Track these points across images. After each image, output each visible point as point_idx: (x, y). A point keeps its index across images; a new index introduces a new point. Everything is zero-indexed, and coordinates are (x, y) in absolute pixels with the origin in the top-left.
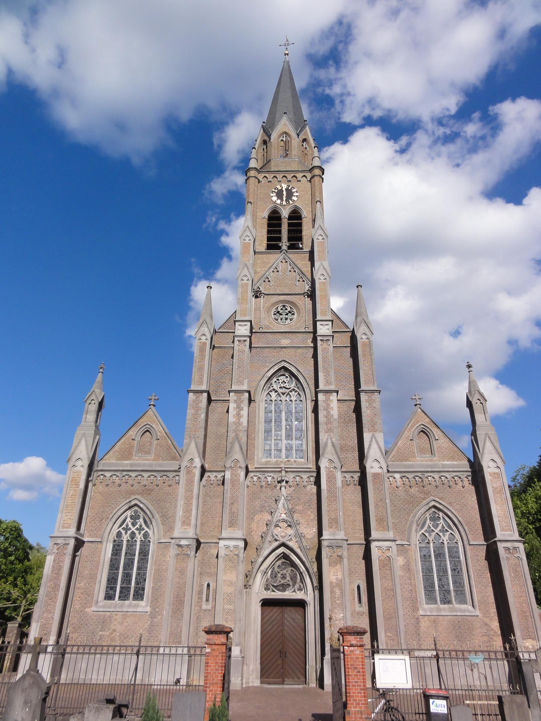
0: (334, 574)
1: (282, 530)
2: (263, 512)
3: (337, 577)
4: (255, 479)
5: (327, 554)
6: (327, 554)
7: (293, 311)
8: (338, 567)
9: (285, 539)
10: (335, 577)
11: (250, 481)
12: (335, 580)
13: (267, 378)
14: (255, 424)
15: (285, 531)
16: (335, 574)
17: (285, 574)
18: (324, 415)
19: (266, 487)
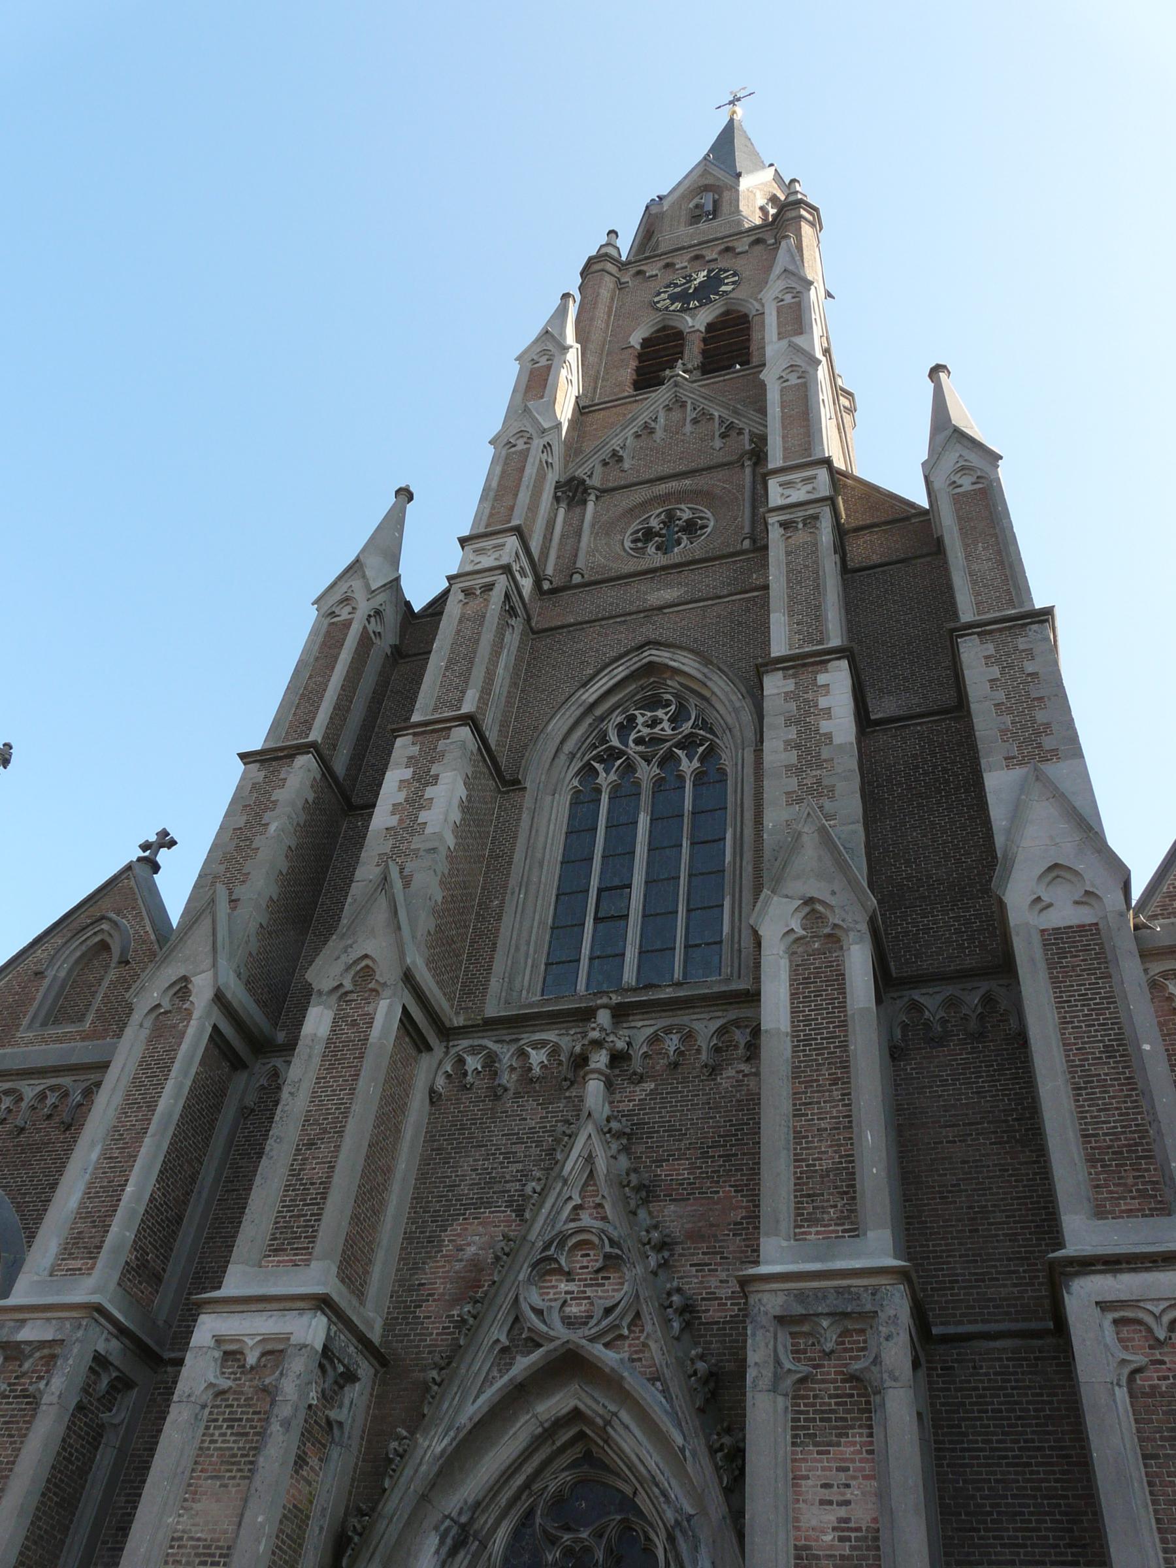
0: (826, 1494)
1: (571, 1287)
2: (488, 1204)
3: (842, 1512)
4: (473, 1063)
5: (778, 1362)
6: (778, 1362)
7: (701, 518)
8: (850, 1448)
9: (580, 1332)
10: (830, 1517)
11: (449, 1076)
12: (828, 1538)
13: (582, 709)
14: (510, 863)
15: (589, 1292)
16: (833, 1495)
17: (587, 1550)
18: (787, 743)
19: (517, 1095)
